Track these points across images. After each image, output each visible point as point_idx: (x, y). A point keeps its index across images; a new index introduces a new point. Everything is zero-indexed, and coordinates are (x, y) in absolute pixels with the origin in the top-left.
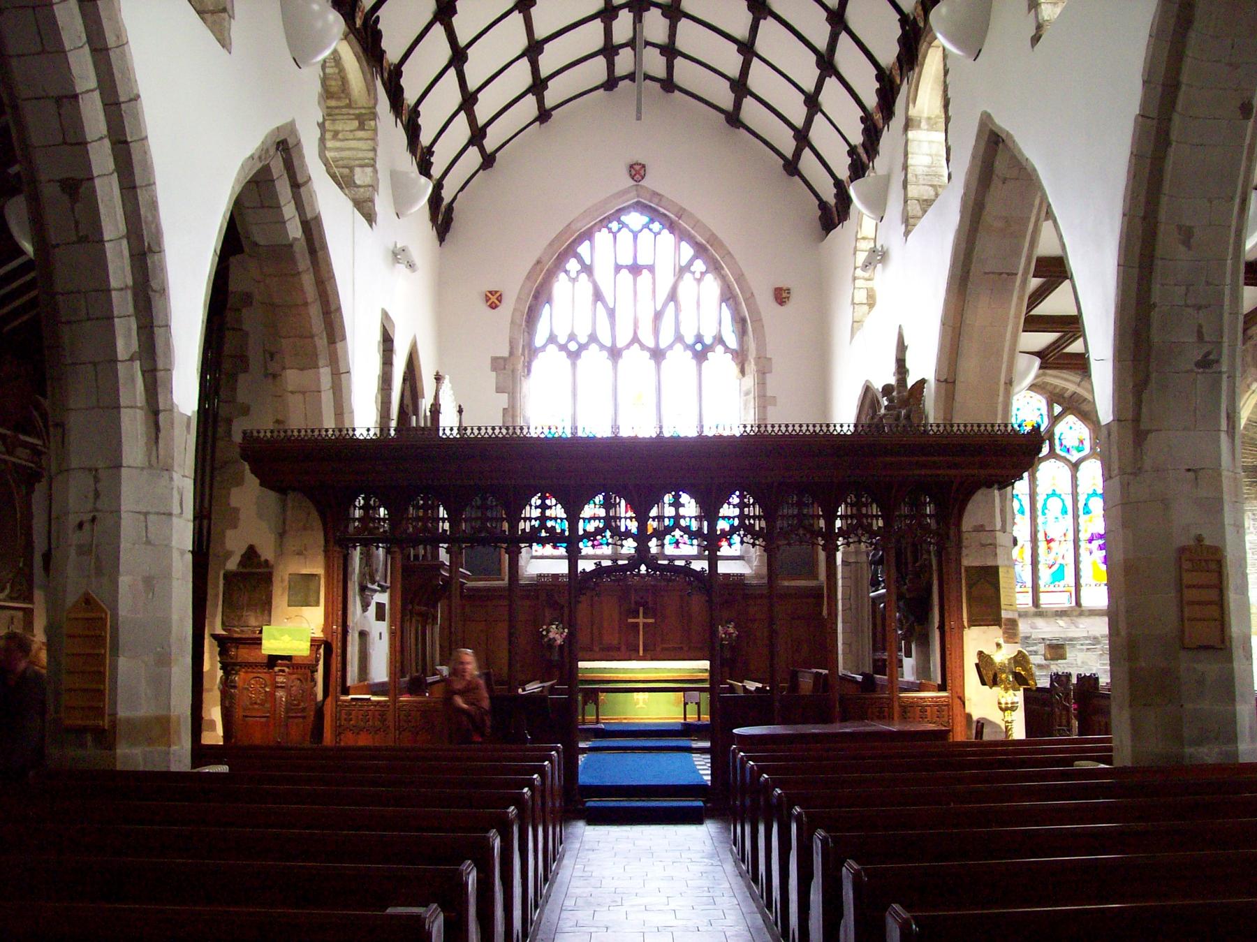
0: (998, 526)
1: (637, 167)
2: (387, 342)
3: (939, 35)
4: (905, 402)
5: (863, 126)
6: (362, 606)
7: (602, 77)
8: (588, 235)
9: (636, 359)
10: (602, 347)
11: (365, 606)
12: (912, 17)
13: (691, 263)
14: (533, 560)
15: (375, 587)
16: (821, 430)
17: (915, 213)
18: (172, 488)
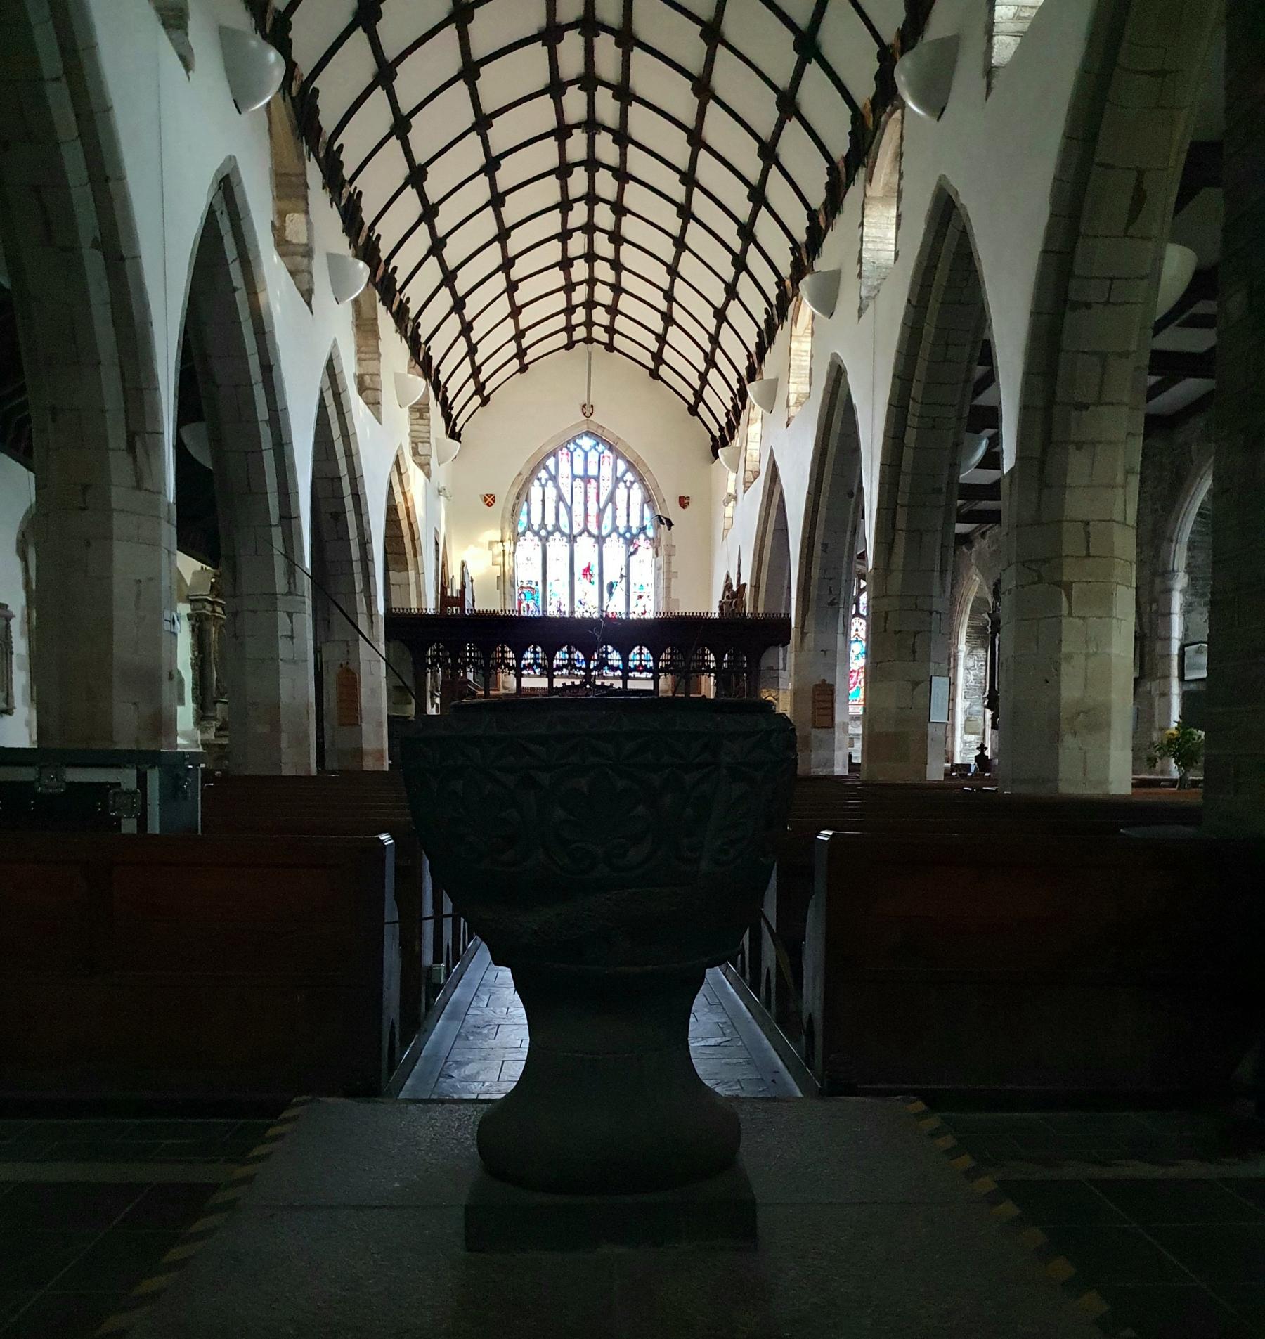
0: (781, 666)
10: (563, 534)
13: (624, 475)
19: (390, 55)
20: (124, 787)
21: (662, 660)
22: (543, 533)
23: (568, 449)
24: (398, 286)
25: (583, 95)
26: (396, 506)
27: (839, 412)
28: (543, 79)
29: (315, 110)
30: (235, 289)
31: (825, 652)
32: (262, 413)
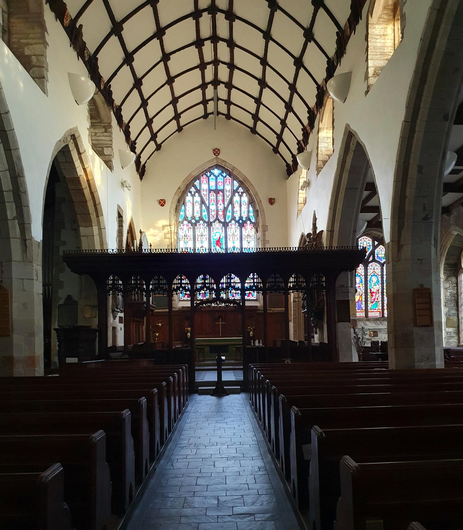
0: (350, 285)
1: (217, 150)
2: (120, 216)
3: (330, 93)
4: (315, 240)
5: (302, 132)
6: (113, 317)
7: (203, 113)
8: (198, 178)
10: (204, 222)
11: (115, 318)
12: (321, 86)
14: (180, 302)
15: (118, 310)
16: (283, 250)
17: (321, 166)
18: (33, 270)
21: (269, 283)
22: (193, 221)
23: (207, 175)
26: (79, 178)
28: (197, 62)
31: (421, 260)
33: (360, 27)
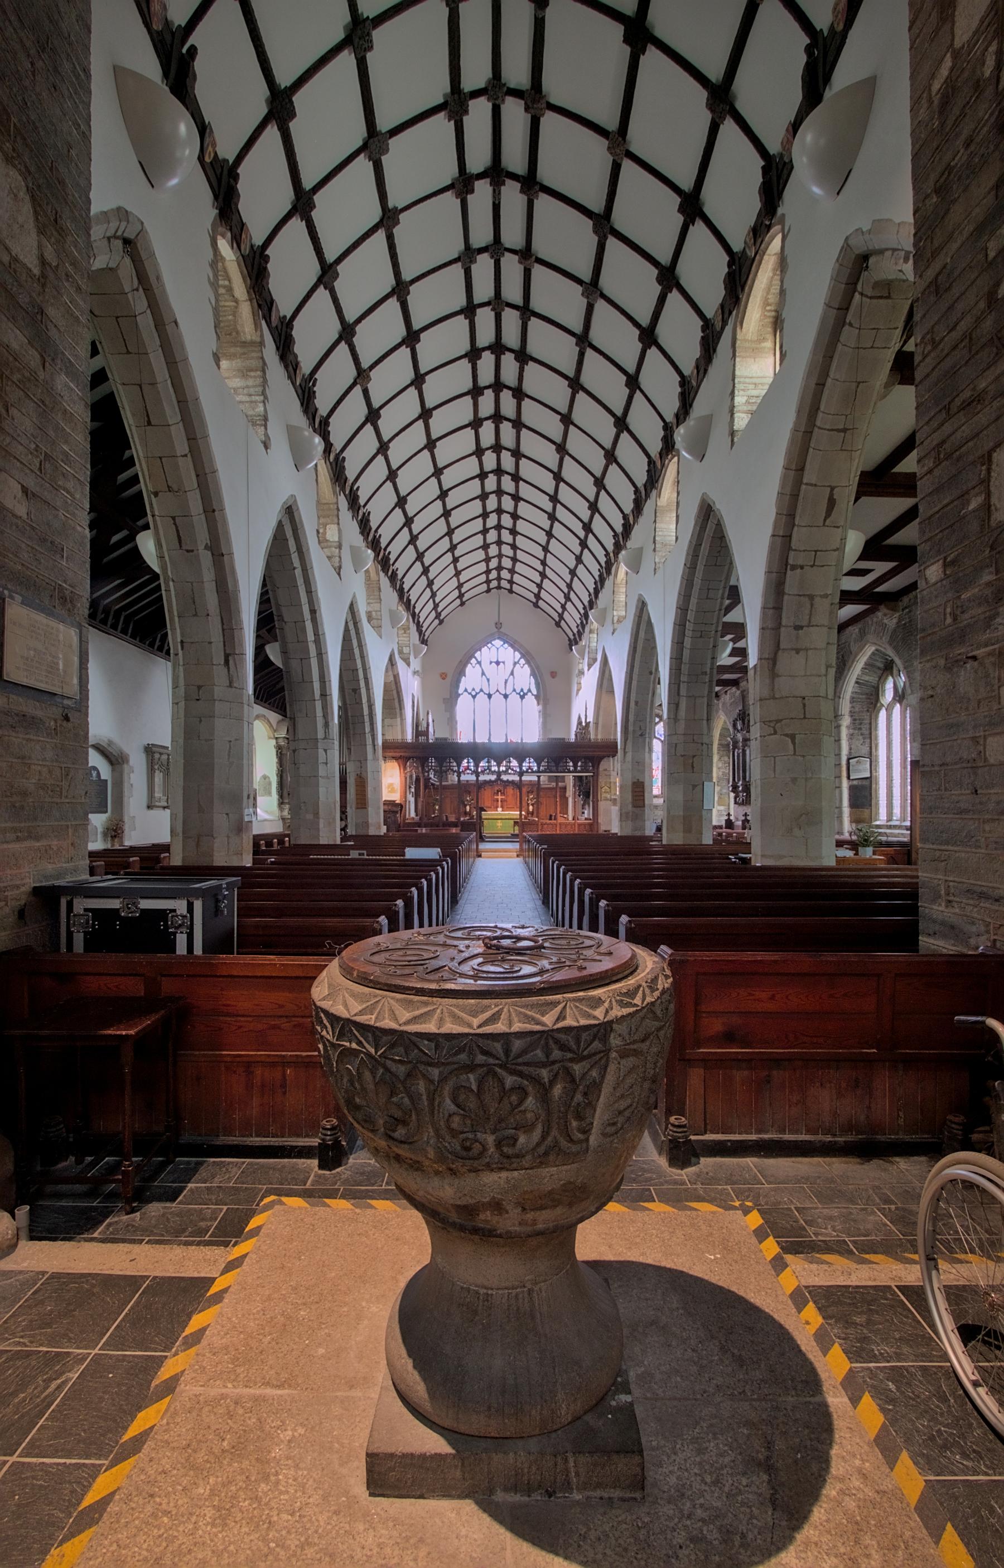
9: (497, 698)
19: (386, 438)
20: (178, 913)
24: (391, 562)
25: (494, 455)
27: (643, 626)
29: (343, 468)
30: (294, 568)
32: (311, 637)
33: (715, 370)
